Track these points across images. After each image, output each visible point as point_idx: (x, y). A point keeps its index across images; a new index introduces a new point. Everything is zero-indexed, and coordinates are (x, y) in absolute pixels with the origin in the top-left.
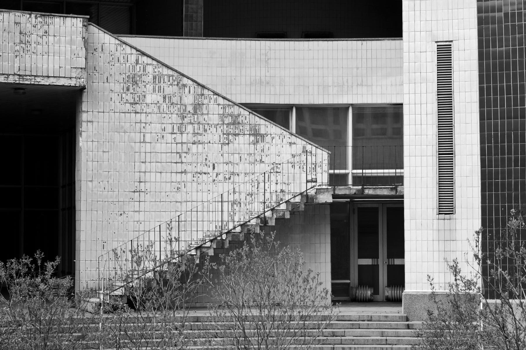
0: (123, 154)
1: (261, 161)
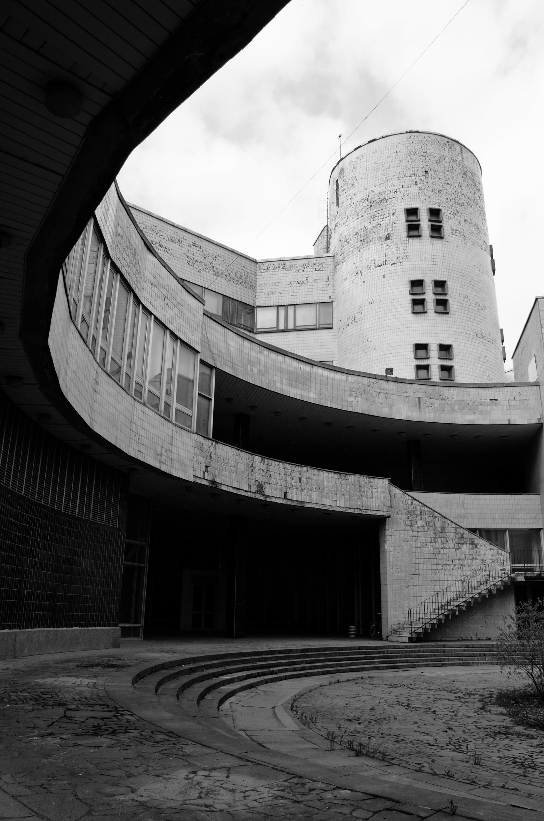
0: (407, 554)
1: (476, 559)
